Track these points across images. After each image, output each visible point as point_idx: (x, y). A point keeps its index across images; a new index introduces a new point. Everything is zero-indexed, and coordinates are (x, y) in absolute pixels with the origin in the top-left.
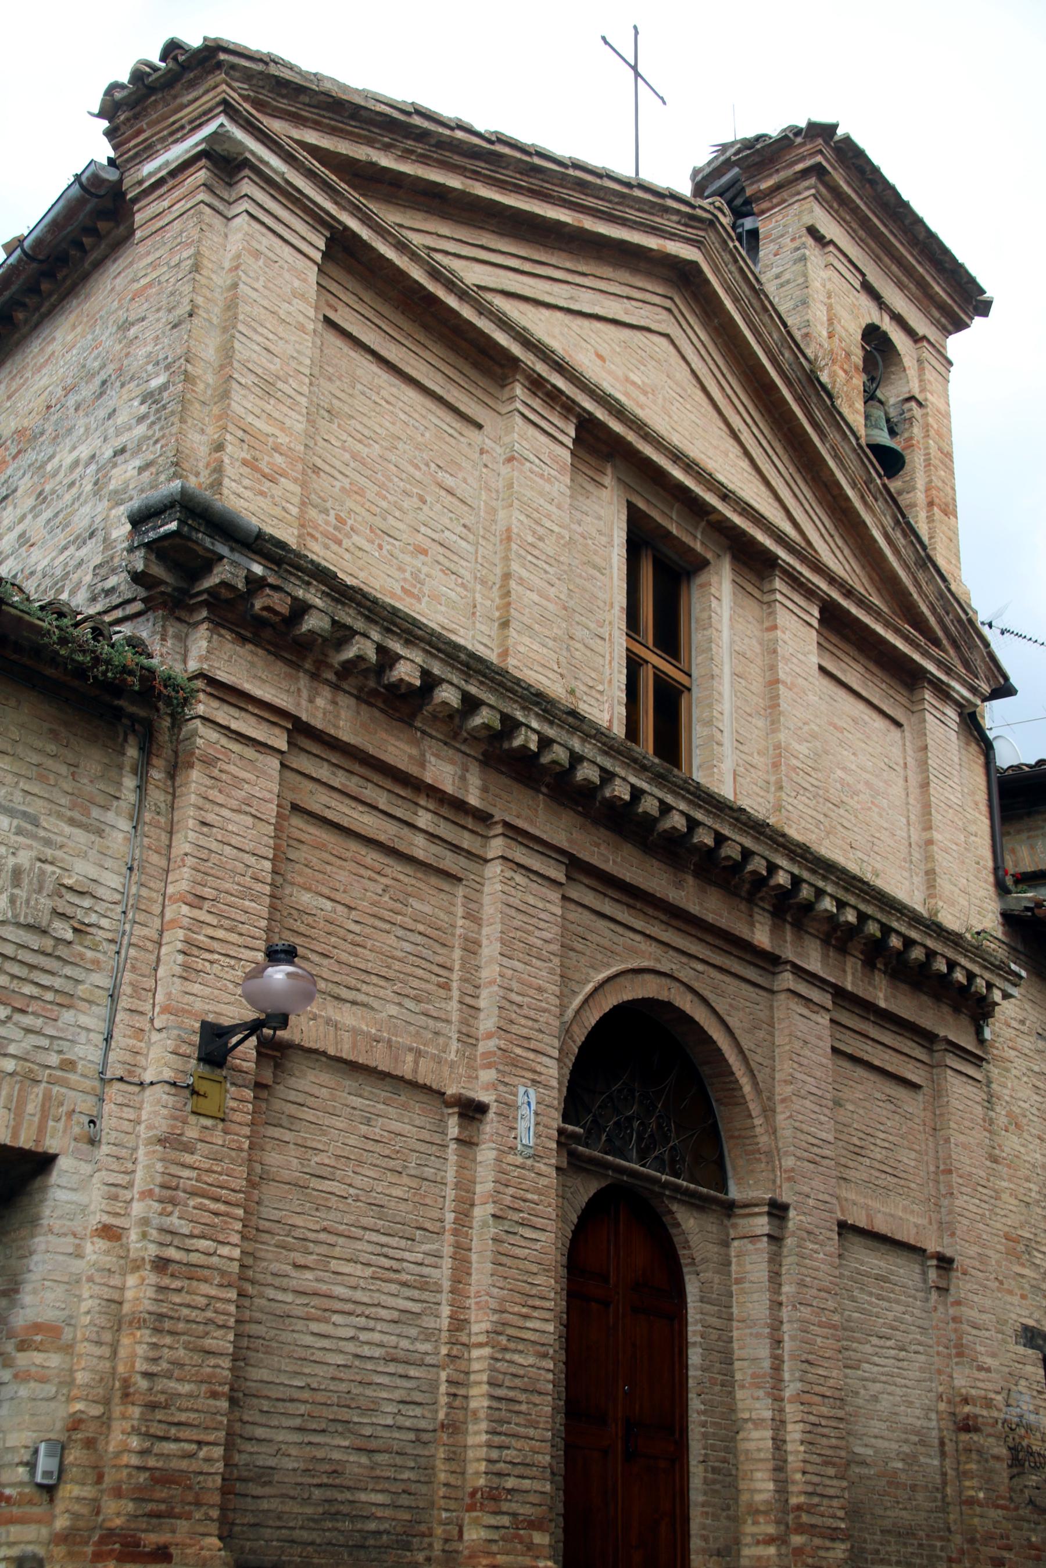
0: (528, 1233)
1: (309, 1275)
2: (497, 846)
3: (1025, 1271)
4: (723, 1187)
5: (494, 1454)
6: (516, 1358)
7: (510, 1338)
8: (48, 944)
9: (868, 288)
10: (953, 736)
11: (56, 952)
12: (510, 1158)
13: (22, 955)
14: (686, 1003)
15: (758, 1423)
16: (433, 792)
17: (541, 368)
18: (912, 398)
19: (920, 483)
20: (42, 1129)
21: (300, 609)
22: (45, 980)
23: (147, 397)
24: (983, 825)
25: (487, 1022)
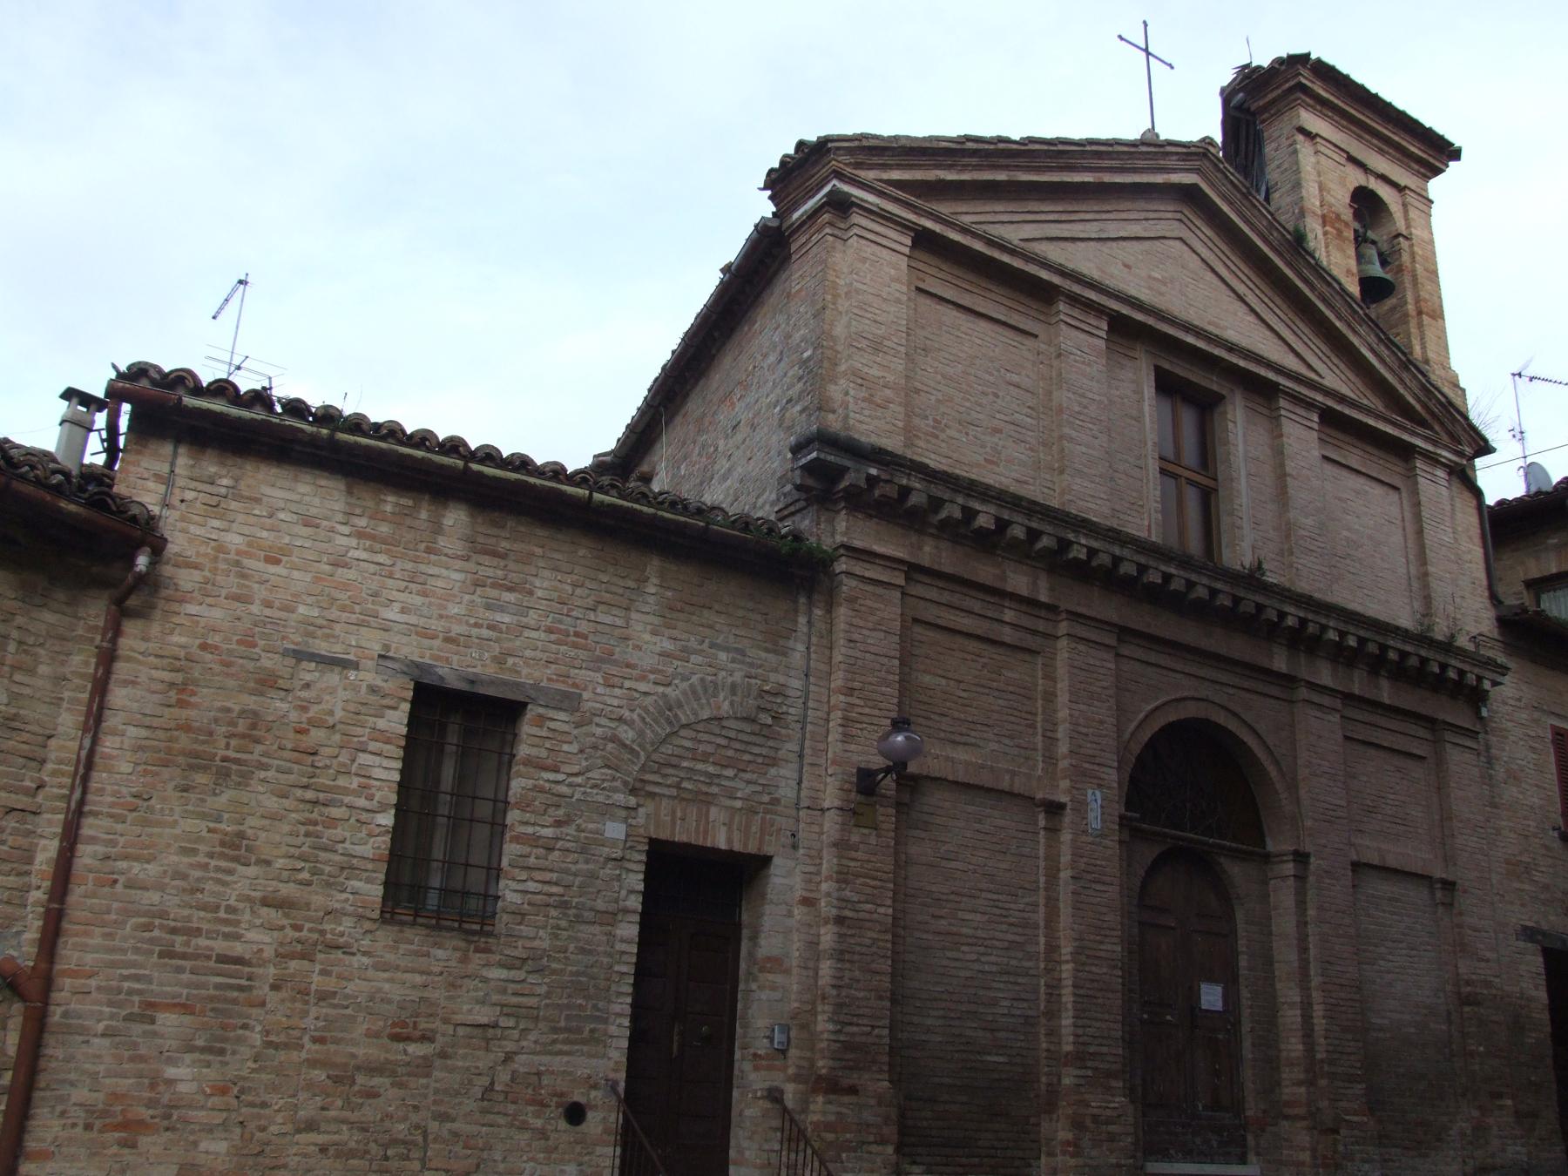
0: (1098, 887)
1: (943, 922)
2: (1063, 627)
3: (1527, 887)
4: (1263, 844)
5: (1080, 1031)
6: (1094, 969)
7: (1088, 957)
8: (757, 728)
9: (1351, 159)
10: (1444, 492)
11: (766, 733)
12: (1084, 838)
13: (740, 736)
14: (1221, 718)
15: (1292, 1005)
16: (1013, 597)
17: (1077, 289)
18: (1399, 235)
19: (1410, 298)
20: (761, 841)
21: (905, 492)
22: (756, 750)
23: (804, 363)
24: (1478, 552)
25: (1063, 748)
